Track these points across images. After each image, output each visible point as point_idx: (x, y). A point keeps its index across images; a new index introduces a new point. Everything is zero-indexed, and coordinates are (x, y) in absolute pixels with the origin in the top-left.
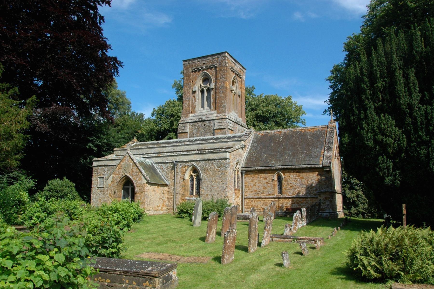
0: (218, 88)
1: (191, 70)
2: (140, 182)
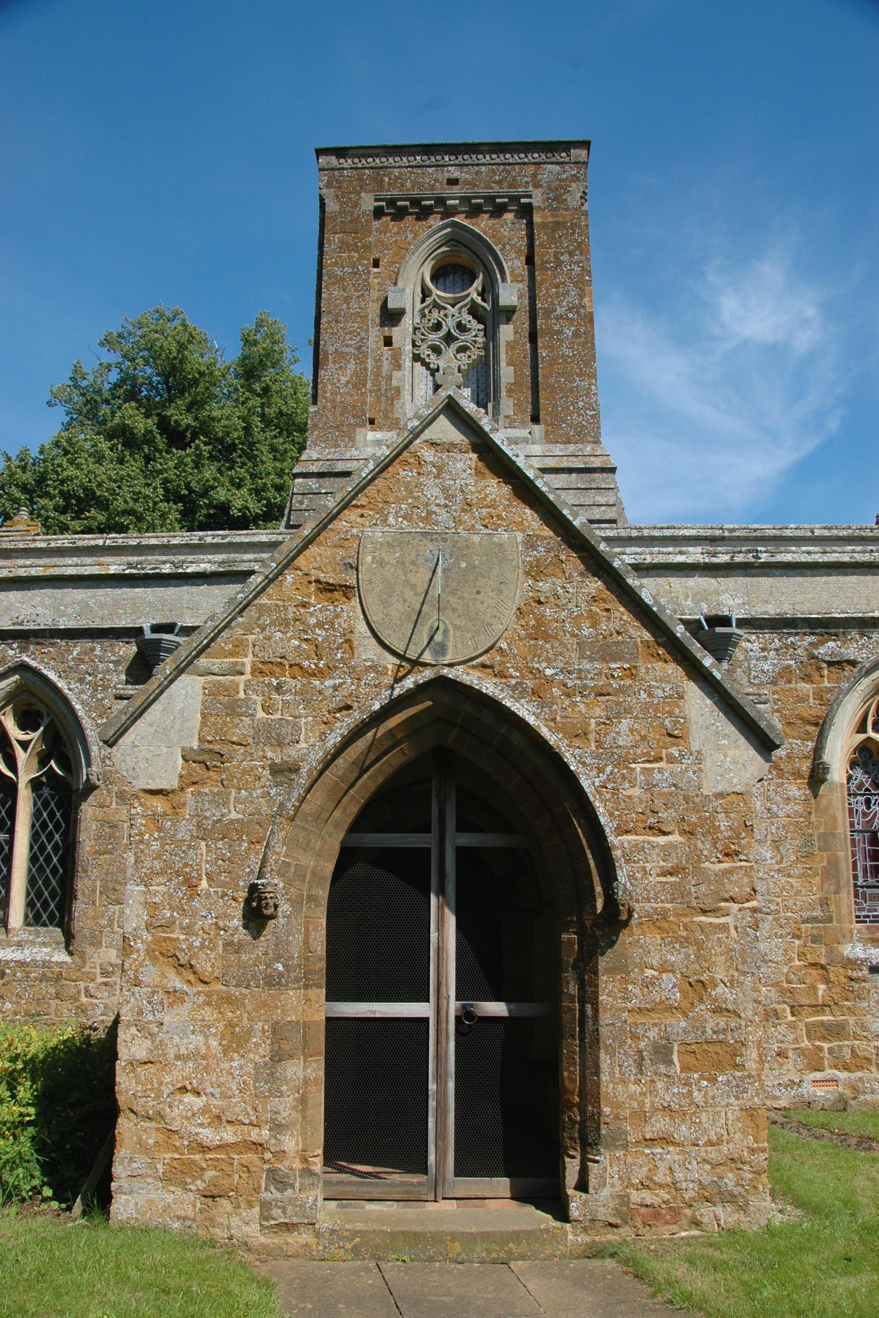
0: (548, 313)
1: (368, 203)
2: (663, 772)
